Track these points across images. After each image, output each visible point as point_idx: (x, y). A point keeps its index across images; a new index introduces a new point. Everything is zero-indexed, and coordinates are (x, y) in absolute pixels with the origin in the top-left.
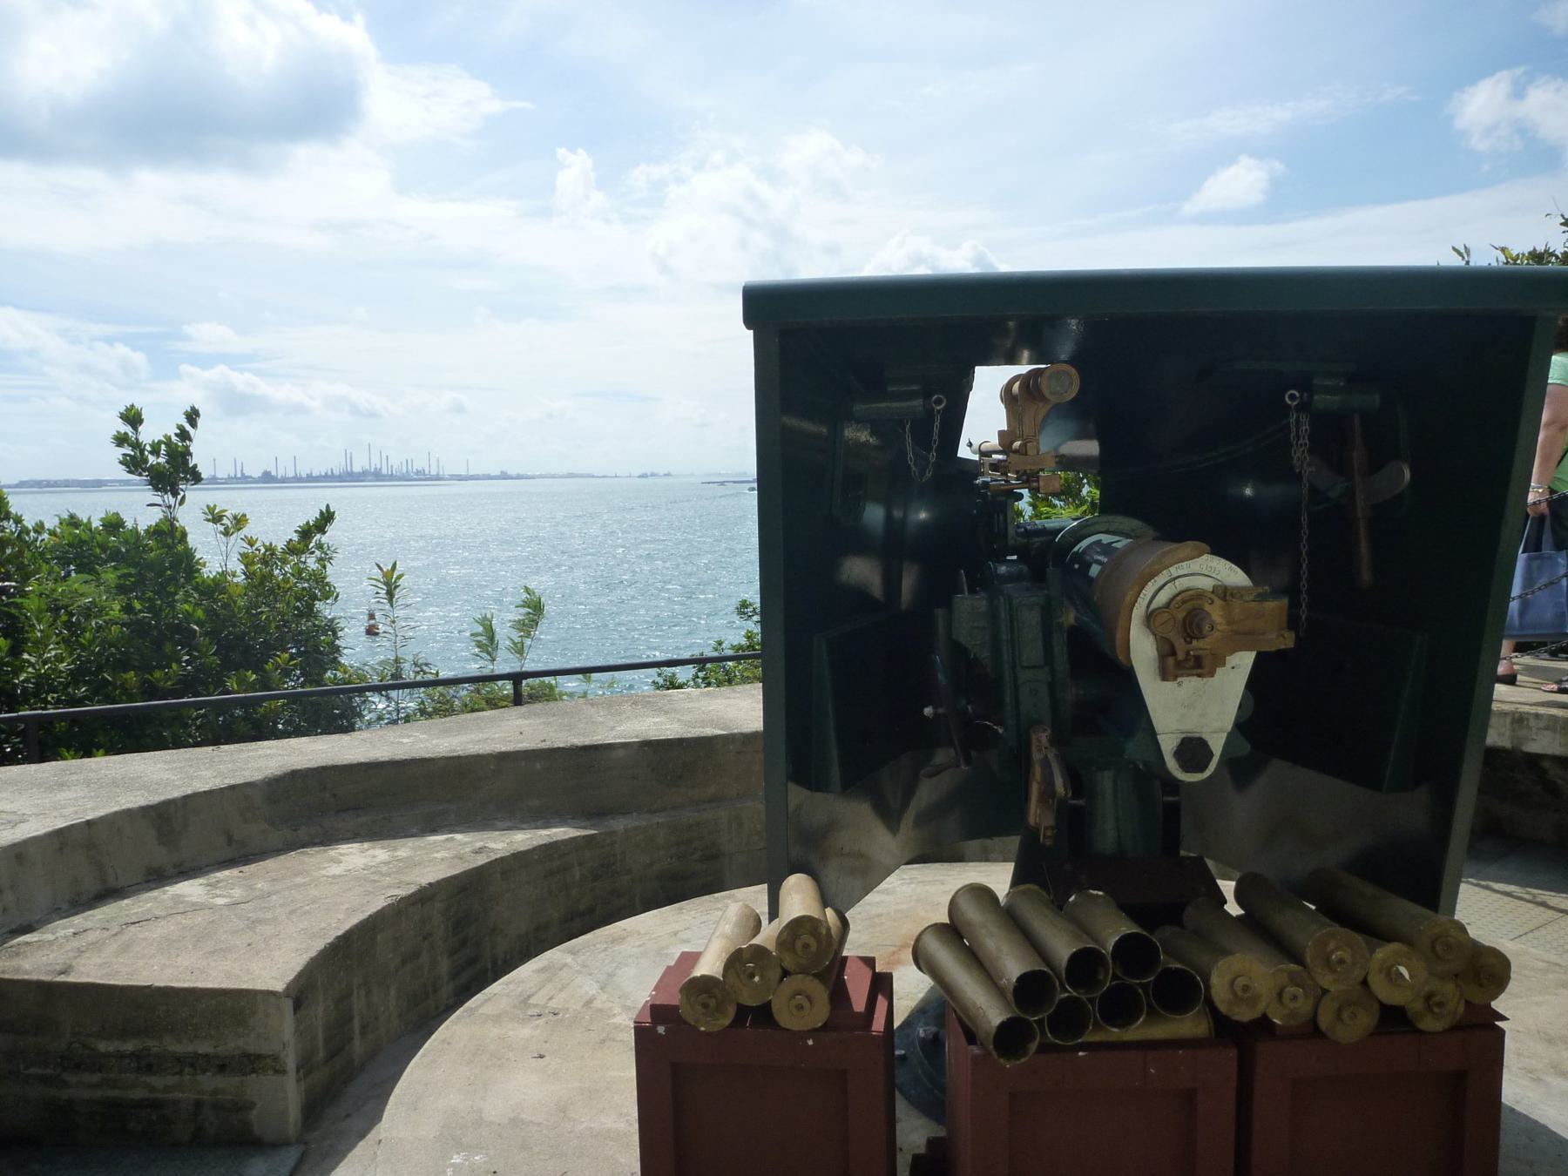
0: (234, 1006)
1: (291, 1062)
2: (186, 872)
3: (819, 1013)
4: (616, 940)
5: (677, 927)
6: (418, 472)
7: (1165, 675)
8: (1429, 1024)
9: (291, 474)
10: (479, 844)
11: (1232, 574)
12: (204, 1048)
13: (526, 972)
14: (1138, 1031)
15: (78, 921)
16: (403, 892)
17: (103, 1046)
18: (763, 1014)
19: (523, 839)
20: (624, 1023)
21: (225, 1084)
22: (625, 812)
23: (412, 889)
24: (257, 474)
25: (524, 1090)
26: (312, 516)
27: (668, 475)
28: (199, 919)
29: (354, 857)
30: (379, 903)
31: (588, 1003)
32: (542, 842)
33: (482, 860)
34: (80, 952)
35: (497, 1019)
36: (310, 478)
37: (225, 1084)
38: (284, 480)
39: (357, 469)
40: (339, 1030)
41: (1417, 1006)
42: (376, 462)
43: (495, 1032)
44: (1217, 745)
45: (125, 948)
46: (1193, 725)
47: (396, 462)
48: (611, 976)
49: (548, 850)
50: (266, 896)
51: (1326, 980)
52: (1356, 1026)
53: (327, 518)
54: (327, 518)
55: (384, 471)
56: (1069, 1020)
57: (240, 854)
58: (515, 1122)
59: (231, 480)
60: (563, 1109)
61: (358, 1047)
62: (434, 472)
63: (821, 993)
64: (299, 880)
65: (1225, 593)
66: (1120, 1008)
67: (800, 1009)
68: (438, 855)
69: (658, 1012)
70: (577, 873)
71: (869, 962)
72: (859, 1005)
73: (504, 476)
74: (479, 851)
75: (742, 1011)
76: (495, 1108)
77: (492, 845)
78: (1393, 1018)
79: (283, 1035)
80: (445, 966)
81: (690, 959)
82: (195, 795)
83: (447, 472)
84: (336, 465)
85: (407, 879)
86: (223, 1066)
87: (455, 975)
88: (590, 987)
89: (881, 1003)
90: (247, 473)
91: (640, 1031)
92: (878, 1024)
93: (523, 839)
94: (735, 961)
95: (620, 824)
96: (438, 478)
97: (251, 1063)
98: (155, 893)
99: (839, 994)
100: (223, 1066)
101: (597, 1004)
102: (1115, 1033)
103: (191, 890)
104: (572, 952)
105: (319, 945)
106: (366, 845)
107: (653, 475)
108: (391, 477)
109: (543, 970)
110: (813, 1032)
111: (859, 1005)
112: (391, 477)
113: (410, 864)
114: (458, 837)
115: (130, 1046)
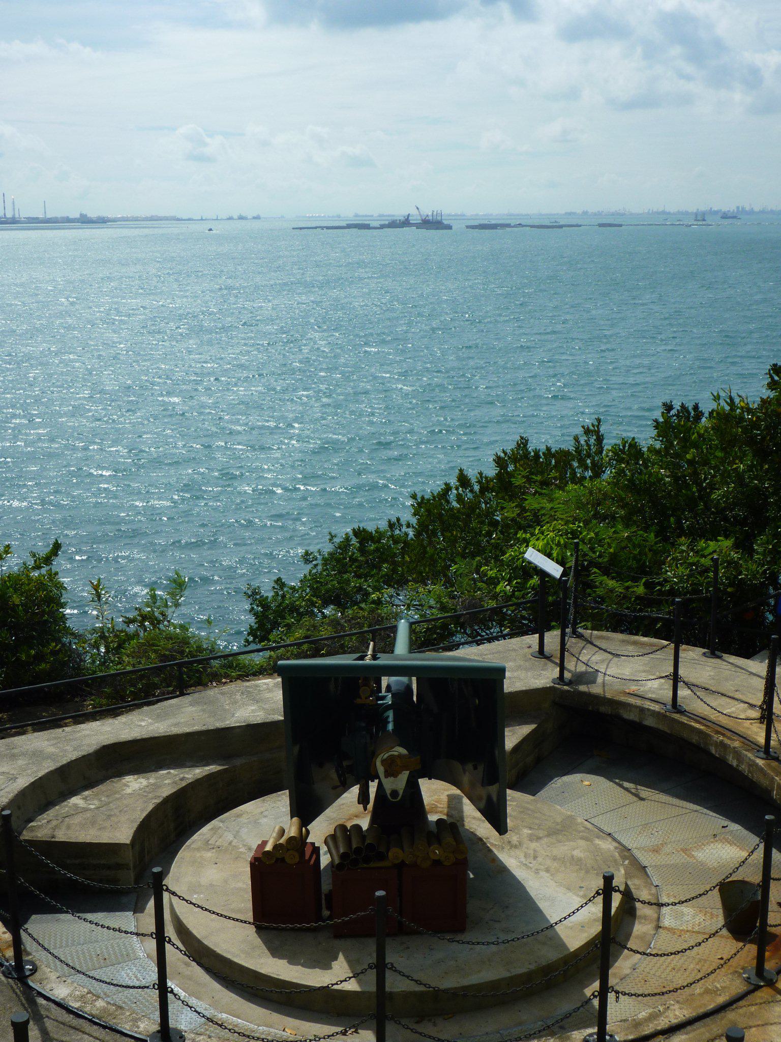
3: (297, 860)
4: (239, 816)
5: (262, 809)
7: (386, 777)
8: (446, 863)
10: (182, 776)
11: (403, 751)
13: (205, 830)
14: (372, 865)
16: (158, 801)
18: (283, 860)
19: (198, 772)
23: (161, 799)
25: (212, 875)
27: (257, 218)
28: (88, 814)
29: (133, 784)
30: (150, 807)
31: (230, 843)
32: (206, 773)
33: (184, 784)
34: (54, 829)
35: (198, 849)
43: (198, 855)
44: (401, 792)
45: (68, 827)
46: (394, 787)
48: (238, 832)
60: (226, 881)
63: (297, 855)
64: (117, 796)
68: (166, 782)
72: (307, 857)
73: (85, 220)
74: (182, 779)
75: (277, 860)
76: (204, 881)
77: (187, 776)
78: (437, 863)
79: (129, 857)
81: (265, 843)
82: (72, 762)
83: (24, 214)
85: (158, 794)
86: (109, 868)
88: (229, 837)
89: (314, 856)
91: (251, 864)
92: (312, 862)
93: (198, 772)
95: (238, 762)
97: (119, 866)
98: (65, 803)
99: (302, 854)
100: (109, 868)
101: (233, 844)
103: (76, 800)
104: (222, 821)
106: (136, 776)
107: (241, 218)
109: (212, 829)
110: (295, 864)
111: (307, 857)
113: (156, 787)
114: (172, 771)
115: (77, 862)
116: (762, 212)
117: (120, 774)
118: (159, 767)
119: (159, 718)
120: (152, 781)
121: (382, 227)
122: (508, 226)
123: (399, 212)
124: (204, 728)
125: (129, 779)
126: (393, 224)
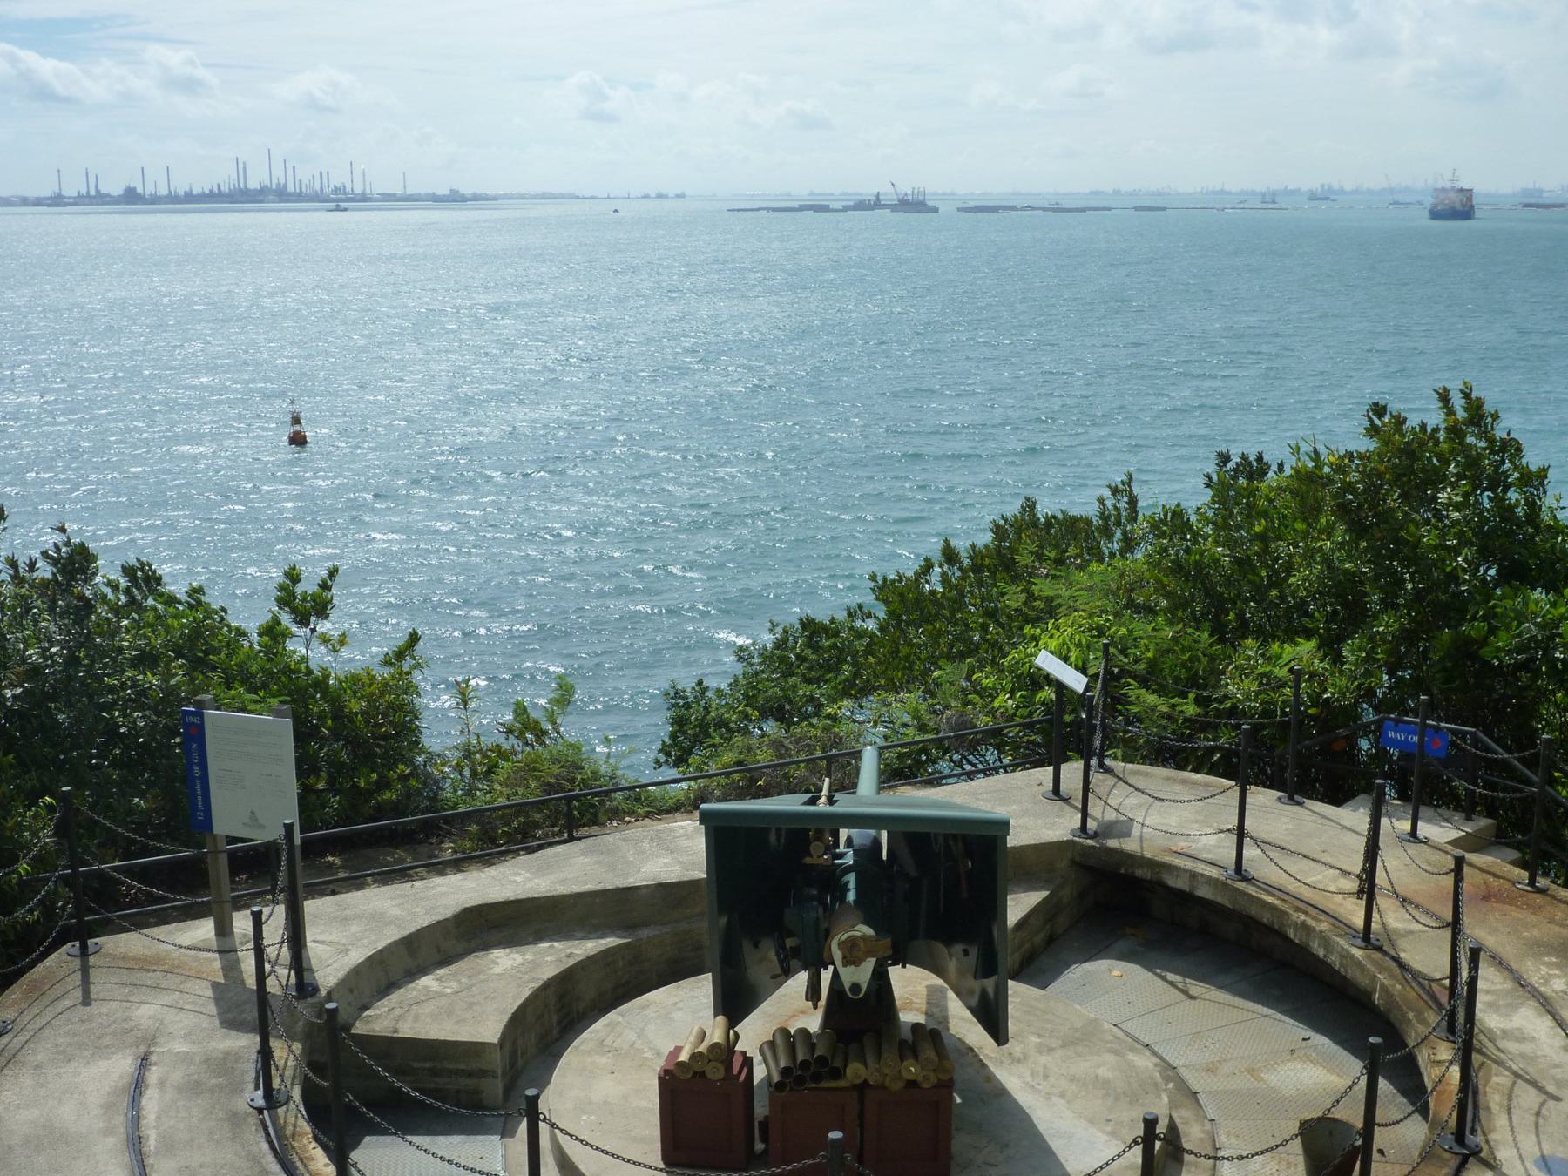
0: (474, 1049)
1: (499, 1072)
2: (423, 971)
3: (721, 1074)
4: (645, 1007)
6: (336, 190)
9: (163, 191)
11: (868, 931)
12: (462, 1066)
13: (600, 1025)
14: (824, 1084)
15: (385, 1001)
16: (537, 985)
17: (416, 1065)
18: (702, 1074)
20: (659, 1065)
21: (471, 1082)
22: (646, 924)
24: (117, 190)
25: (607, 1088)
26: (401, 638)
27: (681, 196)
30: (526, 993)
33: (571, 962)
36: (189, 198)
37: (471, 1082)
38: (155, 199)
39: (253, 184)
40: (514, 1054)
41: (920, 1079)
42: (278, 176)
44: (864, 987)
46: (855, 979)
47: (306, 176)
49: (606, 953)
50: (469, 987)
51: (886, 1071)
52: (897, 1086)
53: (414, 638)
54: (414, 638)
55: (291, 188)
56: (800, 1081)
57: (446, 960)
58: (606, 1103)
59: (82, 200)
61: (520, 1062)
62: (358, 190)
63: (722, 1069)
64: (482, 977)
65: (864, 938)
66: (817, 1078)
67: (715, 1073)
69: (666, 1072)
70: (621, 964)
71: (744, 1053)
73: (456, 198)
74: (569, 956)
75: (695, 1074)
78: (912, 1084)
79: (497, 1062)
80: (555, 1018)
81: (678, 1050)
83: (378, 189)
84: (222, 176)
86: (470, 1074)
87: (559, 1023)
90: (104, 190)
91: (662, 1081)
94: (693, 1056)
95: (645, 933)
96: (364, 198)
97: (483, 1073)
100: (470, 1074)
102: (834, 1084)
103: (427, 981)
105: (505, 1019)
107: (660, 196)
108: (299, 197)
111: (735, 1072)
112: (299, 197)
115: (427, 1065)
116: (1355, 192)
117: (487, 947)
118: (539, 937)
119: (540, 871)
120: (529, 957)
121: (846, 209)
122: (1013, 208)
123: (868, 190)
124: (600, 887)
125: (498, 953)
126: (861, 206)
